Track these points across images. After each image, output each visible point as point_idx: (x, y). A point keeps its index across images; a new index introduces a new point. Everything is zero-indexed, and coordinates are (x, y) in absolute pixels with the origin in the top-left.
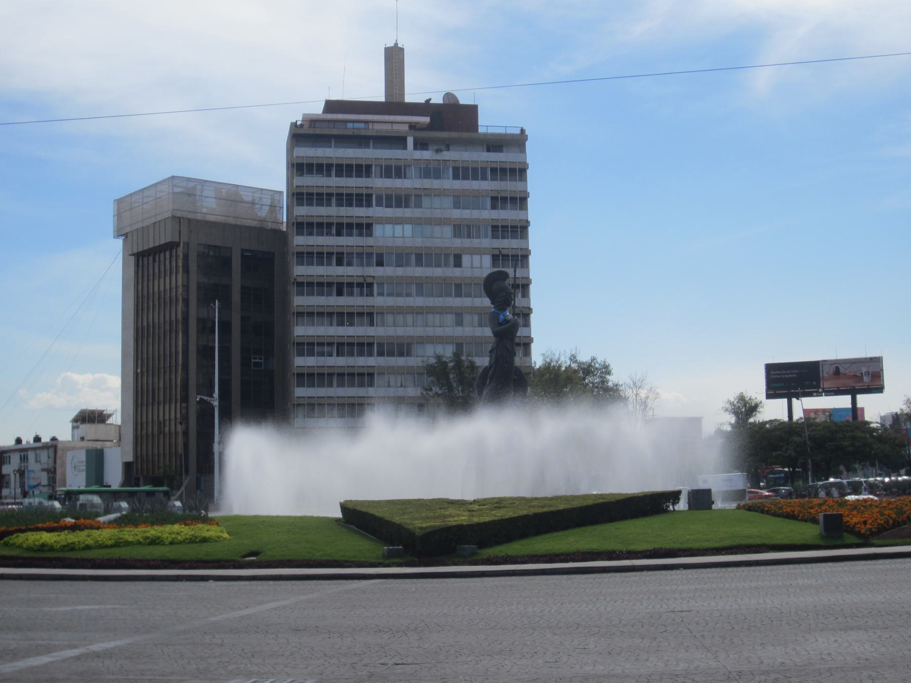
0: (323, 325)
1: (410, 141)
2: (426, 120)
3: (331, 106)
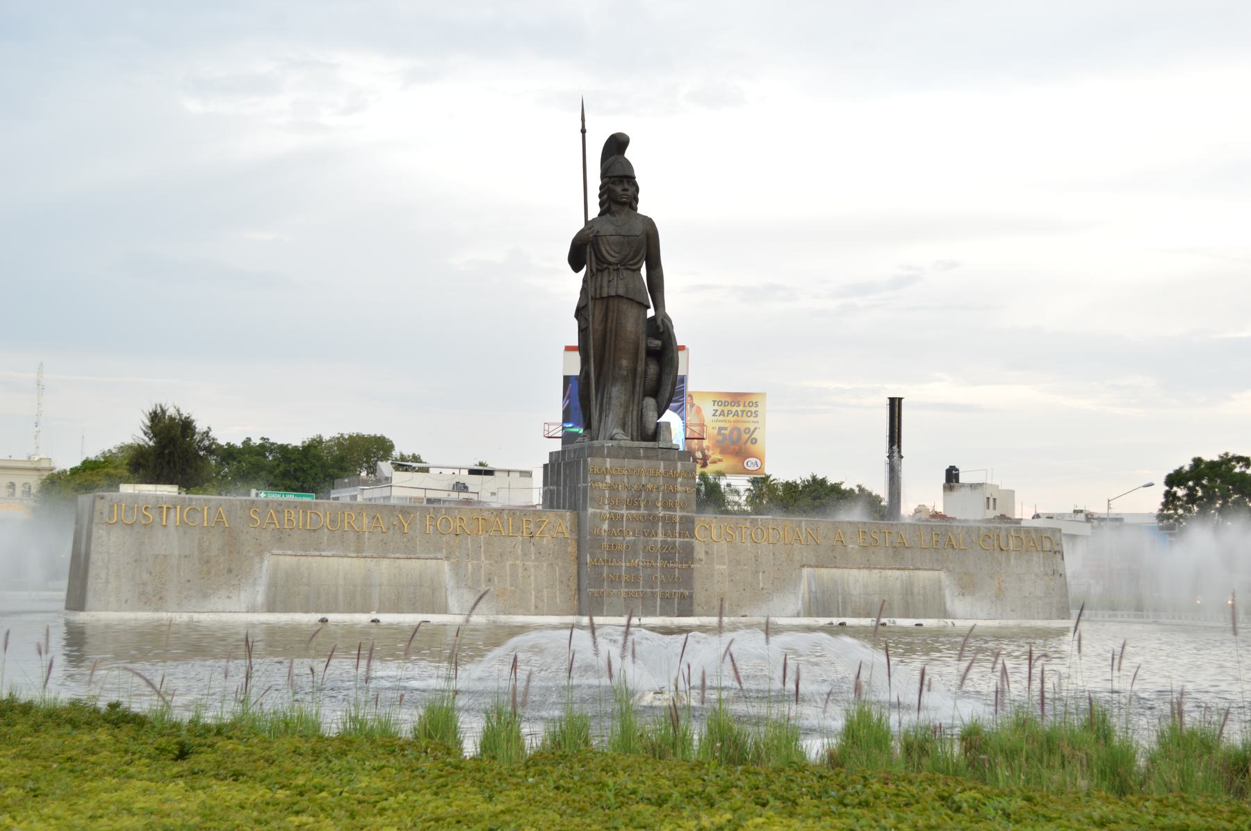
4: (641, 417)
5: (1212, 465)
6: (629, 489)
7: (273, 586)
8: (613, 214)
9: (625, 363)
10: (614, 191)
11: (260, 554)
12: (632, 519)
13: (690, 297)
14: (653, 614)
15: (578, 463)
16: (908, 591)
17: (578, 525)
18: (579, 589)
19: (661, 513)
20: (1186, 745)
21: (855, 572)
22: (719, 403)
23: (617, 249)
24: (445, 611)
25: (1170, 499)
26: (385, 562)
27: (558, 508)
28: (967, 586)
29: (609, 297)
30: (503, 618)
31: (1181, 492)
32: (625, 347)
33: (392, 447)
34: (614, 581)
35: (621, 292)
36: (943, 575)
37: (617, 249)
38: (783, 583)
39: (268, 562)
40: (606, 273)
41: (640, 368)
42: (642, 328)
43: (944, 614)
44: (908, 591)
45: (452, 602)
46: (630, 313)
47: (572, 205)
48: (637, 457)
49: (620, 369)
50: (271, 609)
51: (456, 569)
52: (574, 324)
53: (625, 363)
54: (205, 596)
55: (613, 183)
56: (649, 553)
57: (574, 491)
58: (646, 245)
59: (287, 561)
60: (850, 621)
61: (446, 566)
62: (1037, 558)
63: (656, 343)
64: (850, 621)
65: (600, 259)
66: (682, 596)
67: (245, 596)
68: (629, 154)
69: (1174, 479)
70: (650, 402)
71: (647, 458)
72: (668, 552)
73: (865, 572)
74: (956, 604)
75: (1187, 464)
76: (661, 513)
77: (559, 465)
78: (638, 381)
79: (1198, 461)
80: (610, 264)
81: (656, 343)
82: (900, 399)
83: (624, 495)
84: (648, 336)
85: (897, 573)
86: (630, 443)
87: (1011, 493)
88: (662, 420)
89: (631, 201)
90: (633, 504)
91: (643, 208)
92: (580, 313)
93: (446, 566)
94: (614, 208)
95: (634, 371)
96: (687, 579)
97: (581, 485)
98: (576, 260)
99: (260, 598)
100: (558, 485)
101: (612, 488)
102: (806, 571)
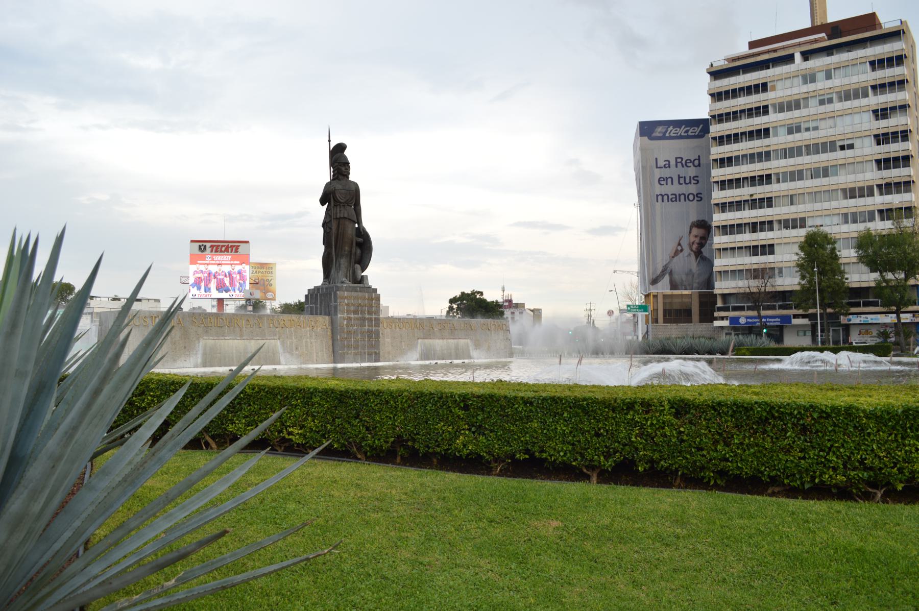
0: (735, 279)
1: (798, 57)
2: (824, 35)
3: (752, 45)
4: (354, 273)
5: (468, 294)
6: (354, 305)
7: (204, 354)
9: (347, 248)
11: (198, 339)
12: (356, 319)
13: (372, 219)
14: (365, 362)
15: (330, 294)
16: (457, 348)
17: (332, 323)
18: (333, 352)
19: (367, 316)
20: (906, 411)
21: (437, 341)
22: (255, 268)
23: (341, 198)
24: (279, 364)
25: (451, 308)
26: (253, 341)
27: (316, 314)
28: (477, 346)
30: (304, 366)
31: (455, 306)
32: (346, 240)
33: (74, 288)
34: (349, 347)
35: (346, 216)
36: (469, 341)
37: (341, 198)
38: (411, 346)
39: (202, 342)
41: (354, 251)
42: (354, 233)
43: (470, 357)
44: (457, 348)
45: (282, 359)
46: (349, 226)
47: (323, 175)
50: (204, 366)
51: (283, 343)
53: (347, 248)
54: (175, 360)
56: (362, 333)
57: (328, 306)
58: (353, 195)
59: (210, 342)
60: (456, 362)
61: (278, 343)
62: (501, 333)
63: (360, 240)
64: (456, 362)
65: (336, 200)
66: (376, 353)
67: (192, 360)
68: (346, 153)
69: (452, 301)
70: (358, 266)
72: (370, 333)
73: (441, 341)
74: (474, 353)
75: (458, 294)
76: (367, 316)
77: (316, 295)
79: (463, 293)
81: (360, 240)
83: (352, 308)
85: (452, 341)
86: (351, 285)
87: (388, 307)
89: (346, 175)
90: (356, 312)
91: (352, 178)
92: (325, 225)
93: (278, 343)
94: (340, 177)
95: (351, 251)
96: (377, 345)
97: (333, 304)
98: (323, 201)
99: (199, 361)
100: (316, 303)
101: (348, 305)
102: (420, 341)
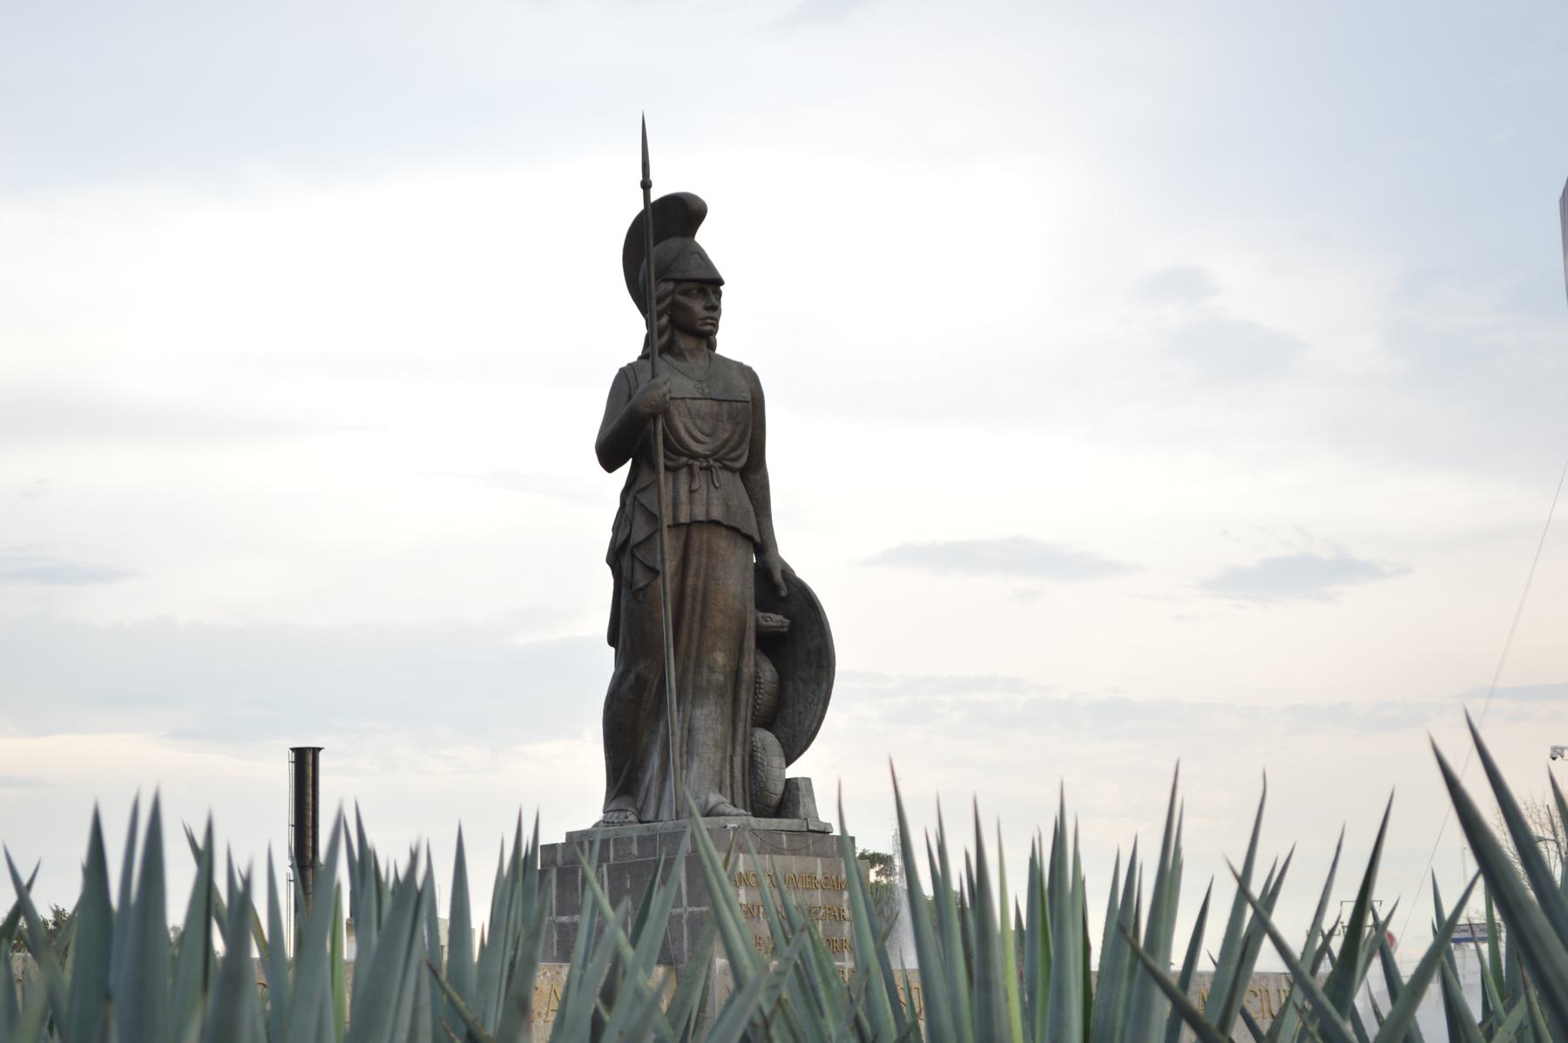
8: (680, 355)
9: (720, 658)
10: (687, 309)
29: (693, 523)
35: (717, 514)
40: (683, 475)
41: (748, 670)
48: (777, 850)
49: (712, 669)
52: (603, 583)
55: (686, 293)
63: (775, 620)
68: (705, 237)
70: (767, 739)
71: (794, 851)
78: (743, 695)
80: (694, 456)
81: (775, 620)
82: (316, 751)
84: (761, 605)
88: (792, 772)
91: (730, 342)
95: (737, 673)
98: (609, 456)
